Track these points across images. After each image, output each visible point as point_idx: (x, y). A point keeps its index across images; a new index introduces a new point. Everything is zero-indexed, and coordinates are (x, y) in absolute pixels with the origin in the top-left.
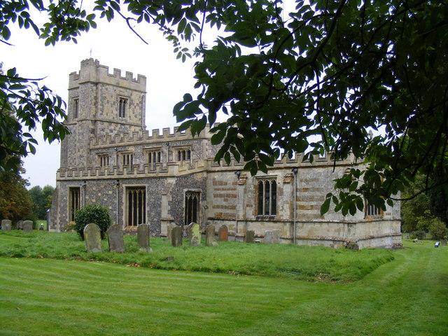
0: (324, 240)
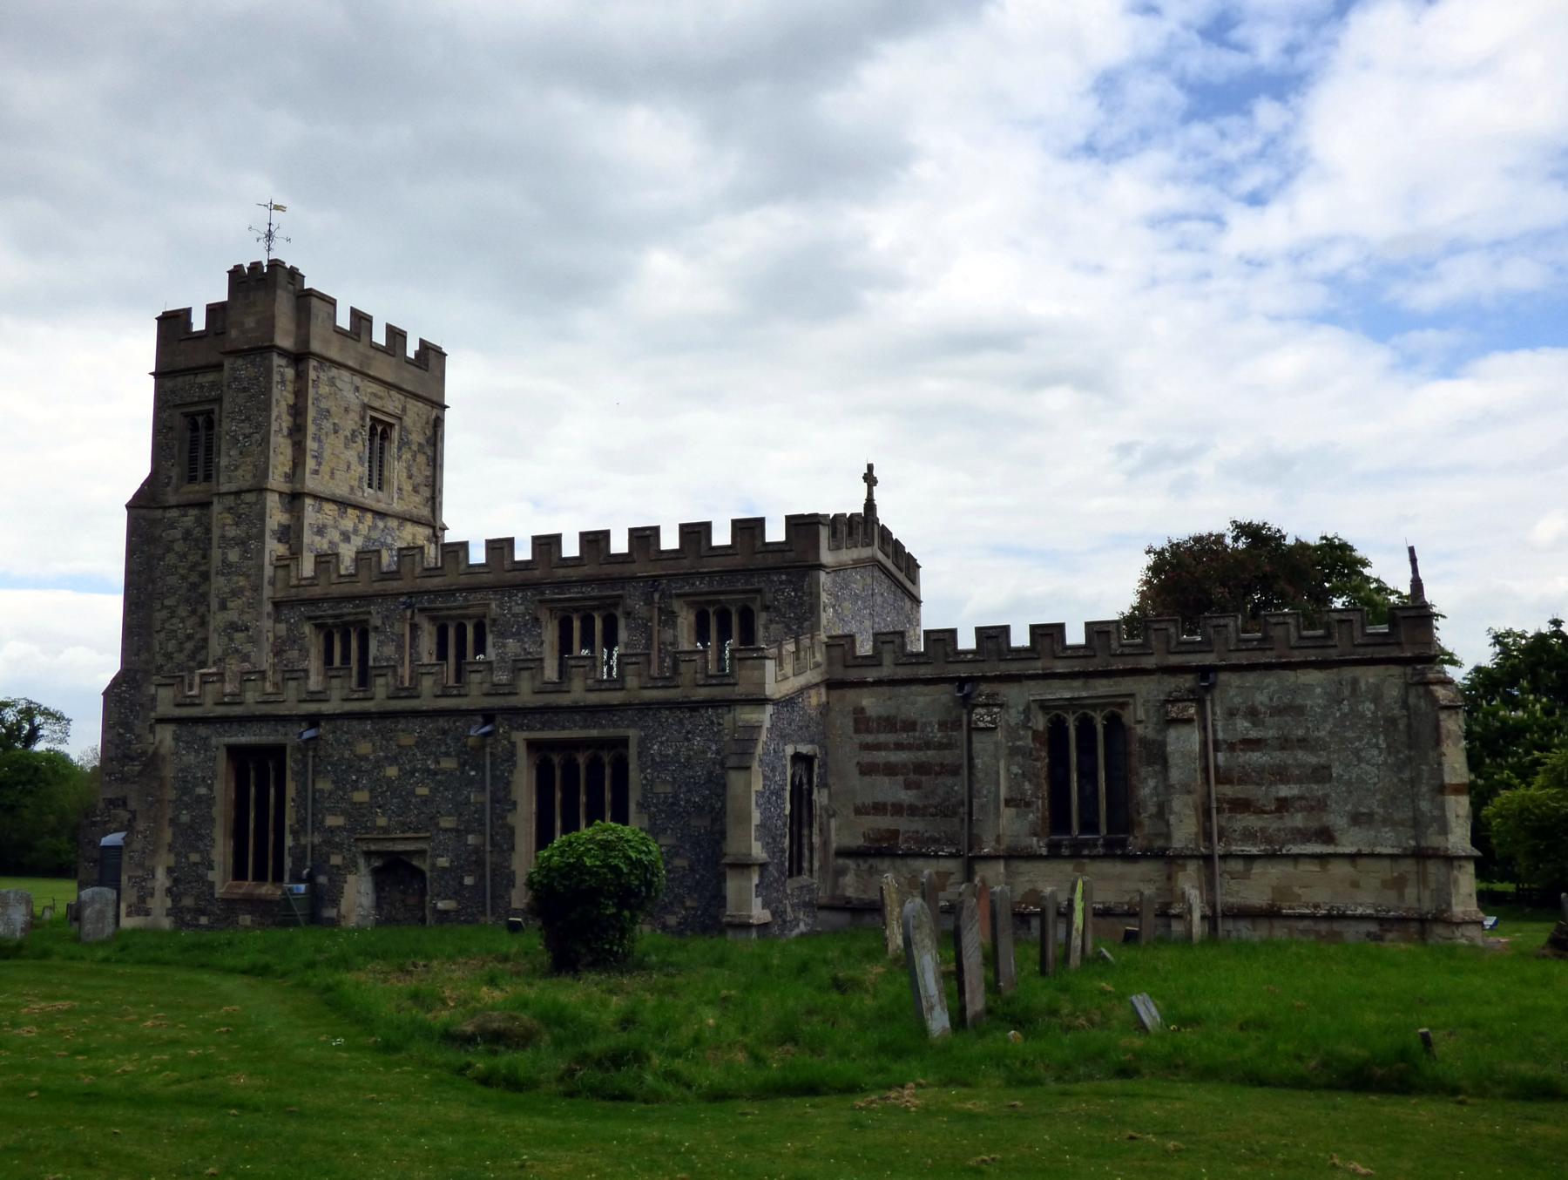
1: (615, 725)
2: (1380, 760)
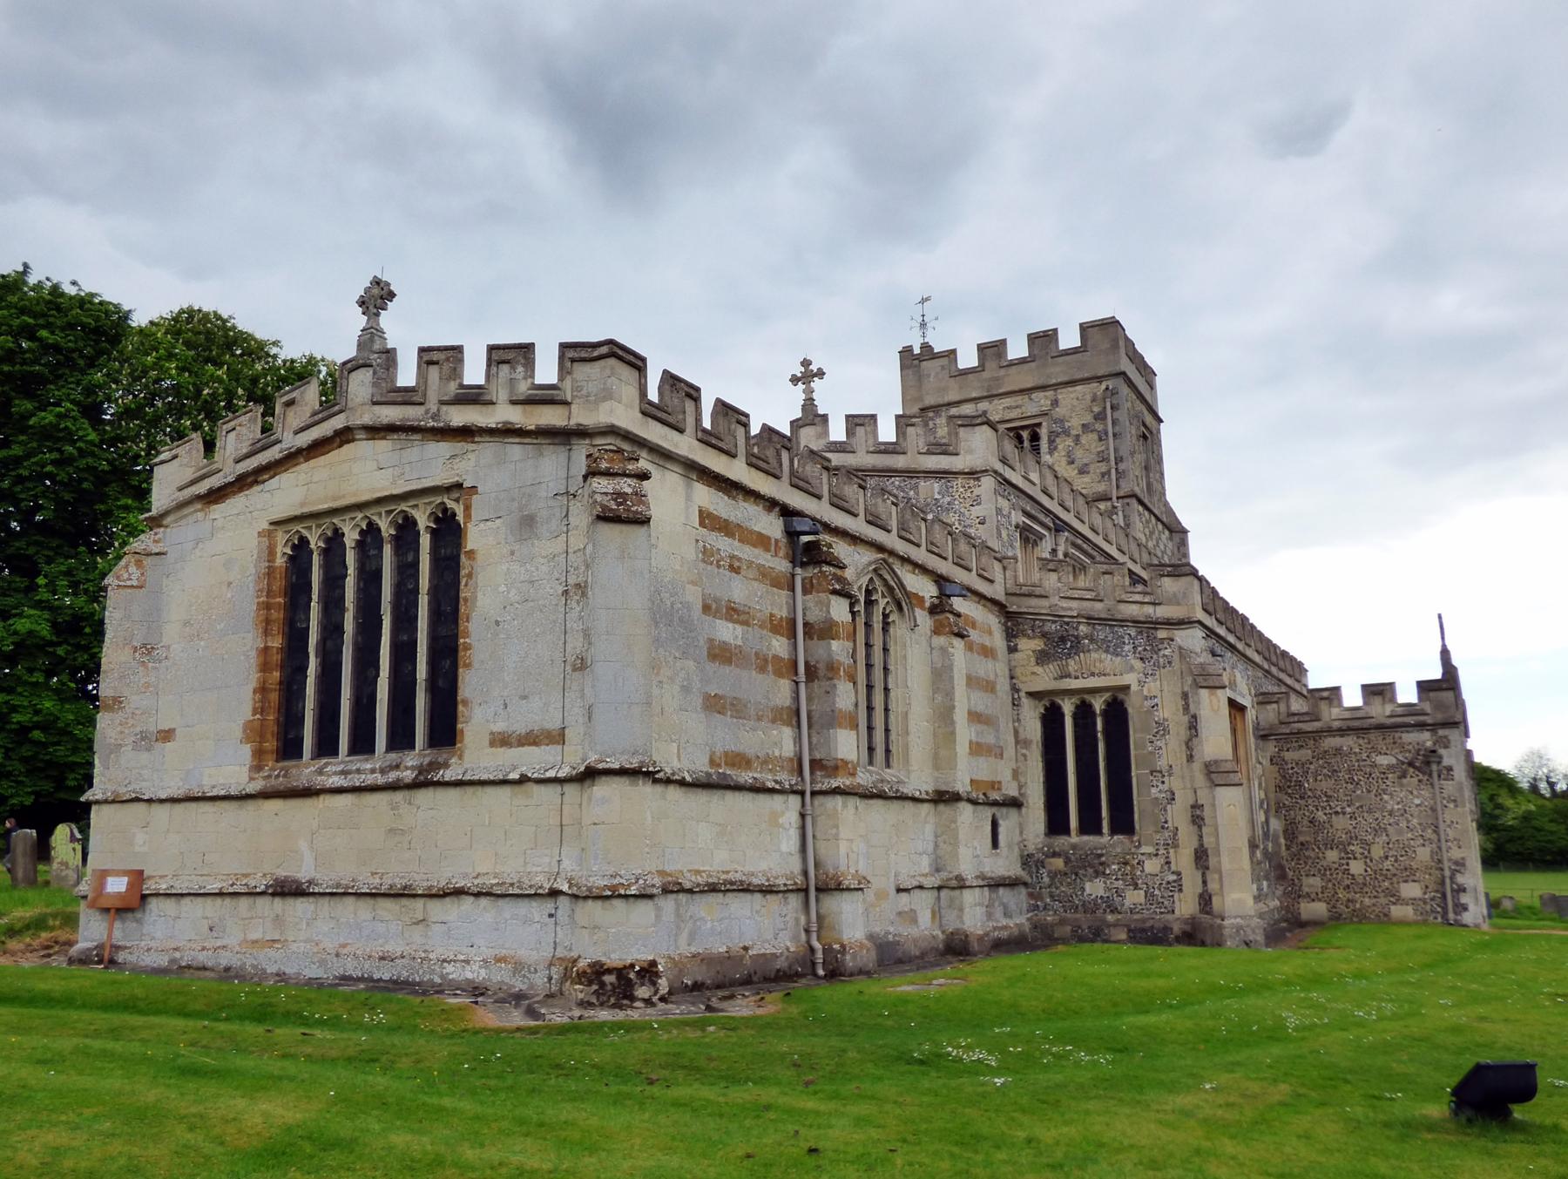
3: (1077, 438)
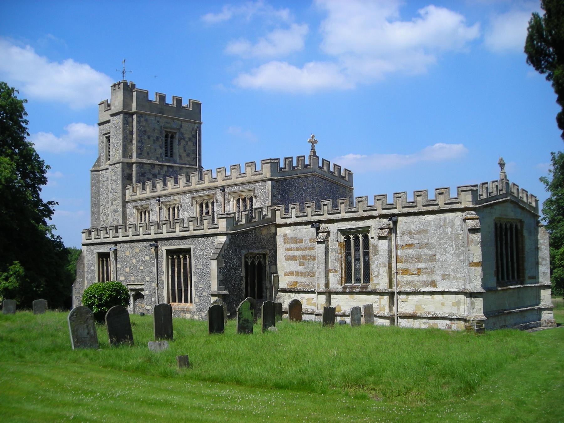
0: (437, 318)
1: (187, 244)
2: (453, 252)
3: (187, 142)
